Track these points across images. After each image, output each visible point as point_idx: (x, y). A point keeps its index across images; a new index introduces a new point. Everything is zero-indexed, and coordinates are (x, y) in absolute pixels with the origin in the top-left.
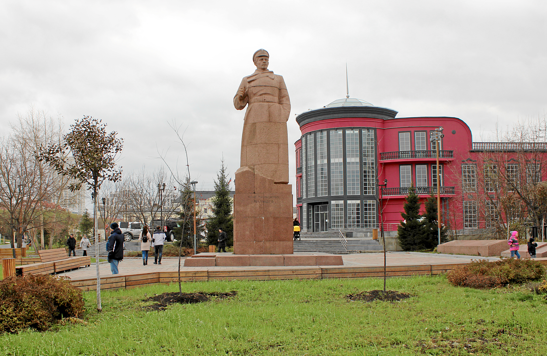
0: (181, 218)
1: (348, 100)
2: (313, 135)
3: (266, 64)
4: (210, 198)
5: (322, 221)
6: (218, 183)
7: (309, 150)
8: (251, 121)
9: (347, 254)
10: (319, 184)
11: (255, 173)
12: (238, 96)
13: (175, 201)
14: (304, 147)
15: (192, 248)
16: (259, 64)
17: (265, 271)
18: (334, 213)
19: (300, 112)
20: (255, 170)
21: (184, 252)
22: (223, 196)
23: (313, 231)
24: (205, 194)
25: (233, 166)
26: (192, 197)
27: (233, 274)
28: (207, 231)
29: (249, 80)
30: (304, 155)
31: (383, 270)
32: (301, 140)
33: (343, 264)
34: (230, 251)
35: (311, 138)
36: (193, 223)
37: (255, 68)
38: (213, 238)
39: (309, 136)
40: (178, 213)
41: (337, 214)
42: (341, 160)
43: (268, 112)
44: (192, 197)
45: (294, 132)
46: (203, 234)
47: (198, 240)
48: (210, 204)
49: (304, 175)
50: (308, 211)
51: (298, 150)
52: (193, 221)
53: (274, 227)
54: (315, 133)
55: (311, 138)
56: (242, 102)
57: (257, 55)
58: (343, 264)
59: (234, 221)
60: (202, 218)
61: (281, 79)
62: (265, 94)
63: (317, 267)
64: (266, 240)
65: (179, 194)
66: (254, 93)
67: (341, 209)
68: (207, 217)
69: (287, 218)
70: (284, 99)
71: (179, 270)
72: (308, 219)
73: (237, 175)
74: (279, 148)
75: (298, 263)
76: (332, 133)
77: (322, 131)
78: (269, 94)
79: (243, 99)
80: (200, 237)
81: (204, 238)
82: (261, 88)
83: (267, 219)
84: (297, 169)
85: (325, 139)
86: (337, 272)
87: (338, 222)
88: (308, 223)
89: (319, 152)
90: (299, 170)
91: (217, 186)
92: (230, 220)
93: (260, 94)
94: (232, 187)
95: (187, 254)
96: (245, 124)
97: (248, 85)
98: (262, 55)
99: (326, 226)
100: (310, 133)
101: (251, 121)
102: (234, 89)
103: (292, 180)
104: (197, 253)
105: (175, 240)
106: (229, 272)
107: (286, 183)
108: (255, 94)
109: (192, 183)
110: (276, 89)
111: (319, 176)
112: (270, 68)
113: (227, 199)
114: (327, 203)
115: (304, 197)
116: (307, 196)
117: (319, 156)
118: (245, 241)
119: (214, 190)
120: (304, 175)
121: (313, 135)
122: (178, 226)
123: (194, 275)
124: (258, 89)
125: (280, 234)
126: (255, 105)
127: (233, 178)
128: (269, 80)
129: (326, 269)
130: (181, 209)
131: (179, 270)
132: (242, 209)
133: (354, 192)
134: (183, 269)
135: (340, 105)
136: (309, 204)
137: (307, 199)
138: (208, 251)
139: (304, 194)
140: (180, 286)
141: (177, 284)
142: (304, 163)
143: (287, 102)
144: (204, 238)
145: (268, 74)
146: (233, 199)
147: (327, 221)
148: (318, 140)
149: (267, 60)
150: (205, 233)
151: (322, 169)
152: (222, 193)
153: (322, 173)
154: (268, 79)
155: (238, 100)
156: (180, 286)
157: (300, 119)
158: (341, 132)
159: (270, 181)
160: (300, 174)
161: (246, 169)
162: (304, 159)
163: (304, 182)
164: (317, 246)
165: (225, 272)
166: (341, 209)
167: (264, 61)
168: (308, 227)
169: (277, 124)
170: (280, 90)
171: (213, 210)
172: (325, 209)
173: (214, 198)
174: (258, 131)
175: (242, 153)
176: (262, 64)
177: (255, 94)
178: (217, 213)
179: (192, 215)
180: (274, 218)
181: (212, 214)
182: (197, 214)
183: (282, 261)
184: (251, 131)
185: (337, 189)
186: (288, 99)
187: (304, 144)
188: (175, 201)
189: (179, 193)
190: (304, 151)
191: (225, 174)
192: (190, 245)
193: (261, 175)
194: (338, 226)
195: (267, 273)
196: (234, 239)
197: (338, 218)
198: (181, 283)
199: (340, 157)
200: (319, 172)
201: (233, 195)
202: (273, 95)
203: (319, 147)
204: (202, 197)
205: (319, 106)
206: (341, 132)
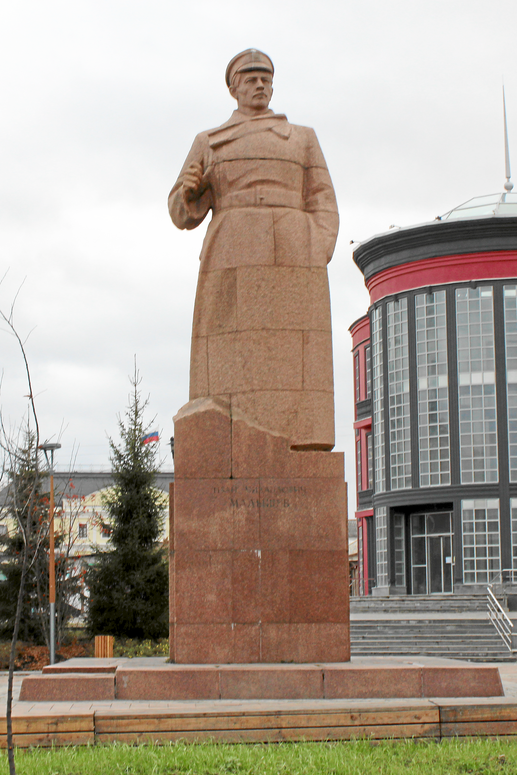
0: (8, 554)
1: (509, 198)
2: (404, 301)
3: (264, 94)
4: (98, 494)
6: (123, 449)
8: (220, 263)
10: (425, 449)
11: (235, 418)
12: (181, 190)
14: (377, 340)
16: (246, 93)
17: (269, 714)
18: (471, 538)
19: (365, 236)
20: (234, 409)
21: (20, 656)
23: (409, 592)
24: (80, 482)
25: (166, 401)
26: (44, 489)
27: (171, 723)
28: (87, 594)
29: (214, 143)
30: (378, 363)
32: (369, 316)
33: (500, 693)
34: (157, 653)
35: (398, 311)
37: (233, 104)
39: (391, 305)
41: (481, 540)
42: (490, 378)
43: (270, 237)
44: (44, 489)
45: (349, 295)
47: (62, 619)
48: (99, 510)
49: (379, 422)
50: (392, 532)
51: (361, 349)
52: (47, 564)
53: (291, 581)
54: (411, 296)
55: (398, 311)
56: (193, 205)
58: (500, 693)
60: (72, 552)
62: (262, 182)
63: (425, 702)
64: (269, 621)
66: (230, 178)
67: (493, 526)
68: (89, 551)
69: (332, 553)
70: (320, 197)
71: (9, 713)
72: (392, 556)
74: (305, 341)
75: (364, 689)
76: (462, 295)
77: (430, 291)
78: (274, 182)
80: (66, 612)
81: (77, 613)
82: (252, 165)
83: (270, 557)
84: (359, 406)
85: (442, 314)
86: (487, 715)
87: (482, 564)
88: (392, 568)
89: (422, 353)
90: (363, 407)
91: (120, 457)
92: (156, 560)
93: (245, 184)
94: (163, 459)
95: (28, 663)
96: (204, 272)
97: (210, 157)
98: (253, 65)
99: (444, 577)
100: (396, 298)
101: (220, 263)
102: (169, 171)
103: (345, 440)
104: (59, 658)
106: (159, 717)
107: (328, 447)
108: (231, 184)
109: (45, 448)
110: (294, 166)
111: (424, 424)
112: (276, 105)
113: (147, 497)
114: (449, 506)
115: (380, 490)
116: (388, 487)
117: (422, 366)
118: (206, 623)
120: (379, 422)
121: (404, 301)
123: (53, 728)
125: (300, 597)
126: (236, 214)
127: (167, 432)
128: (274, 139)
129: (454, 709)
131: (9, 713)
132: (194, 524)
133: (480, 476)
134: (20, 709)
136: (395, 511)
137: (388, 495)
138: (89, 654)
139: (380, 479)
140: (11, 761)
142: (379, 387)
143: (329, 208)
144: (77, 613)
145: (271, 123)
146: (166, 495)
147: (449, 560)
148: (421, 317)
150: (83, 598)
151: (433, 406)
152: (133, 481)
153: (433, 418)
154: (272, 138)
155: (182, 200)
157: (367, 255)
158: (487, 293)
159: (279, 442)
160: (366, 420)
161: (207, 405)
162: (378, 374)
163: (380, 444)
164: (419, 637)
165: (146, 717)
166: (493, 526)
168: (393, 581)
170: (307, 169)
171: (106, 530)
173: (112, 492)
175: (193, 360)
176: (253, 92)
177: (231, 184)
178: (119, 538)
179: (45, 544)
180: (291, 552)
181: (104, 543)
182: (59, 540)
183: (317, 680)
184: (220, 293)
186: (331, 198)
187: (377, 329)
192: (36, 636)
193: (250, 424)
194: (482, 577)
195: (273, 721)
196: (172, 616)
197: (482, 552)
200: (424, 413)
202: (285, 186)
204: (74, 491)
205: (196, 265)
206: (487, 293)
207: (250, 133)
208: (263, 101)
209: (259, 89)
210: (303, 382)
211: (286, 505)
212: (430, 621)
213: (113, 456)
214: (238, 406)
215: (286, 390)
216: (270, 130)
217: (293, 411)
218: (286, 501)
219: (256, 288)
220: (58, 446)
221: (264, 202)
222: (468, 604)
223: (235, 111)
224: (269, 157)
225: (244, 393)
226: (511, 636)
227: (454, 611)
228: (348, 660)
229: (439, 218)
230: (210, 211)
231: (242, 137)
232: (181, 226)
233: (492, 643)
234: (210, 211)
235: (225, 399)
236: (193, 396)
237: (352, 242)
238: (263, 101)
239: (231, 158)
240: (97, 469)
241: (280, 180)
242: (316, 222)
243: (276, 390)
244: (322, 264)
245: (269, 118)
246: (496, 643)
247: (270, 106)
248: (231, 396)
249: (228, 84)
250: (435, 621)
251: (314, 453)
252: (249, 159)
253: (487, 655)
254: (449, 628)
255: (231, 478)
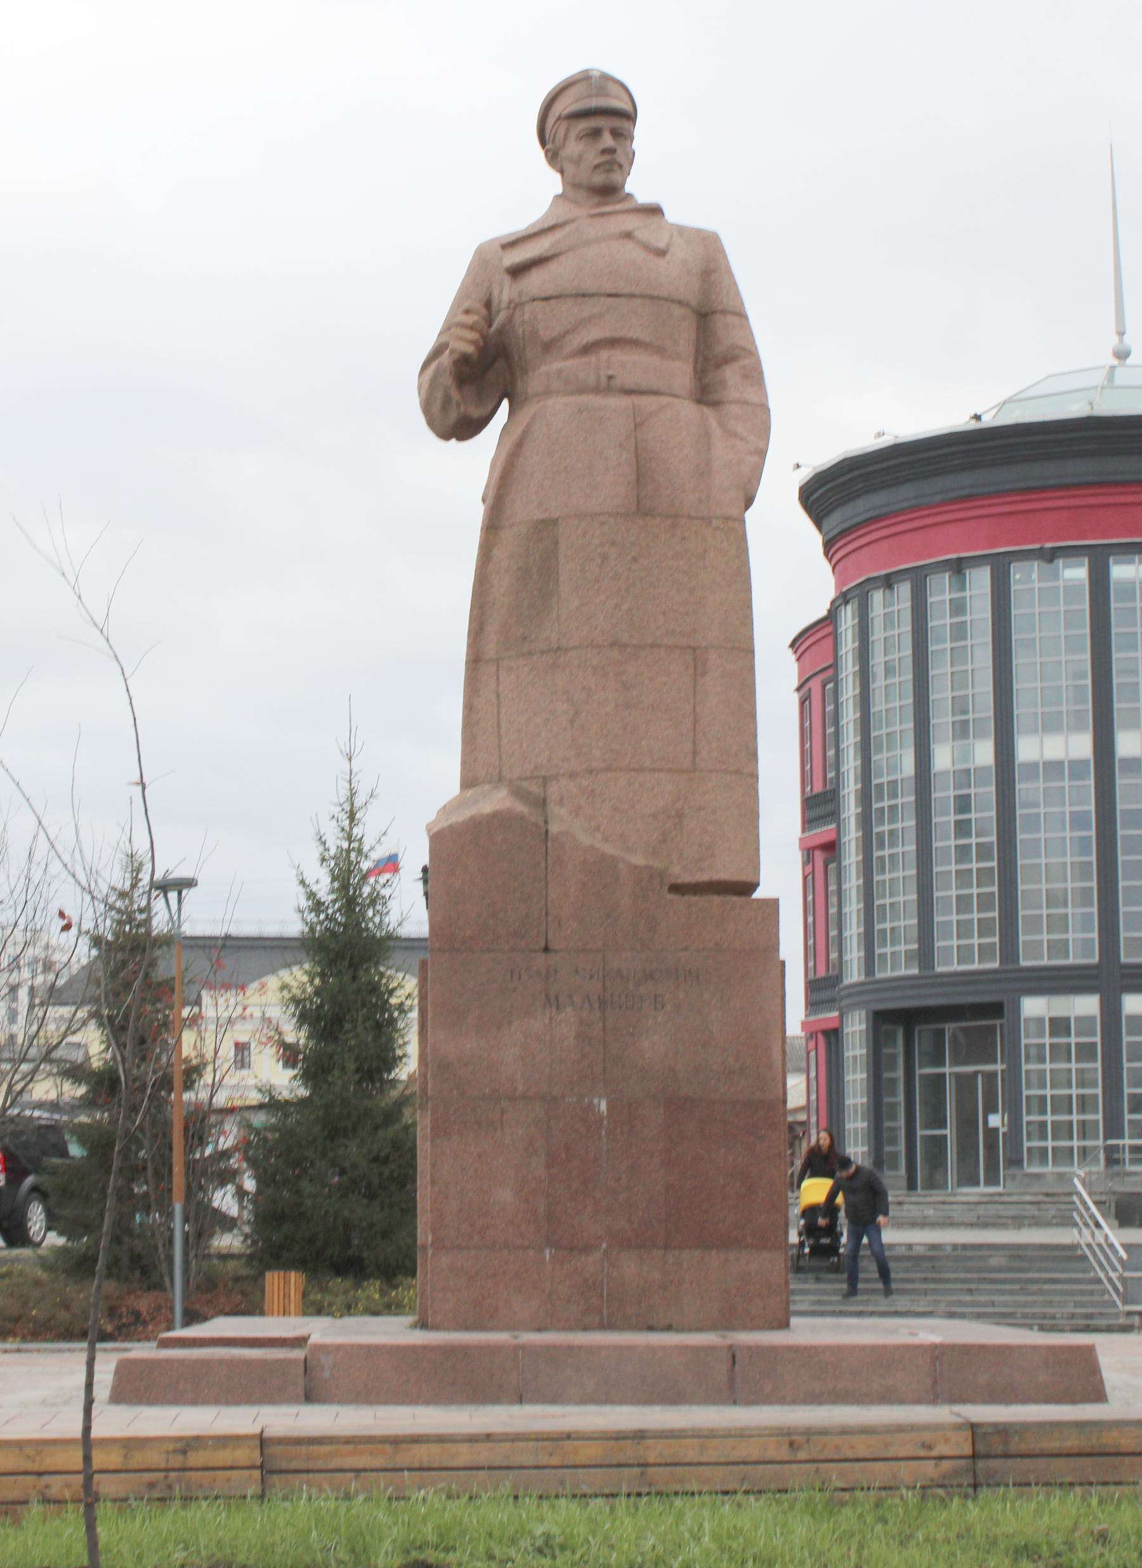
0: (87, 1104)
1: (1121, 377)
2: (904, 590)
4: (273, 982)
5: (967, 1124)
6: (324, 888)
7: (878, 683)
8: (524, 509)
9: (1126, 1329)
10: (946, 892)
11: (554, 828)
12: (445, 359)
13: (54, 996)
14: (849, 668)
15: (158, 1286)
16: (578, 161)
20: (554, 809)
21: (112, 1312)
22: (354, 966)
23: (911, 1185)
24: (236, 957)
25: (416, 785)
28: (250, 1185)
29: (515, 262)
30: (850, 715)
31: (75, 1458)
32: (831, 619)
34: (391, 1308)
35: (891, 610)
36: (166, 1135)
37: (552, 183)
38: (287, 1228)
39: (877, 597)
40: (75, 1072)
42: (1082, 746)
45: (789, 571)
46: (224, 1200)
47: (199, 1236)
48: (275, 1013)
49: (851, 836)
50: (877, 1064)
51: (815, 685)
52: (168, 1124)
54: (919, 579)
55: (891, 610)
57: (565, 106)
58: (1098, 1395)
59: (422, 1123)
60: (220, 1100)
61: (710, 261)
62: (613, 343)
65: (85, 953)
66: (546, 334)
67: (1085, 1052)
68: (254, 1098)
70: (730, 373)
71: (87, 1429)
73: (439, 840)
74: (698, 669)
76: (1026, 578)
77: (958, 567)
78: (635, 343)
79: (475, 376)
80: (210, 1221)
81: (227, 1223)
82: (590, 308)
85: (981, 610)
89: (941, 694)
90: (819, 805)
91: (318, 906)
92: (392, 1115)
93: (579, 351)
94: (406, 910)
95: (126, 1326)
96: (492, 526)
97: (506, 291)
98: (594, 103)
100: (888, 582)
101: (524, 509)
102: (422, 313)
103: (781, 875)
104: (192, 1317)
105: (55, 1240)
107: (747, 888)
108: (548, 347)
110: (677, 311)
111: (945, 842)
112: (640, 185)
113: (374, 988)
114: (995, 1010)
115: (854, 975)
116: (869, 969)
117: (942, 719)
119: (294, 927)
120: (851, 836)
121: (904, 590)
122: (75, 1150)
123: (177, 1461)
124: (568, 312)
126: (555, 411)
127: (416, 855)
128: (638, 255)
129: (1003, 1430)
130: (93, 1044)
131: (87, 1429)
134: (115, 1422)
135: (1075, 409)
136: (885, 1021)
137: (871, 986)
138: (253, 1307)
139: (854, 954)
140: (91, 1528)
141: (73, 1517)
142: (851, 764)
143: (751, 395)
145: (630, 223)
147: (995, 1121)
148: (940, 621)
149: (623, 135)
150: (241, 1193)
152: (344, 951)
153: (962, 828)
154: (630, 252)
155: (448, 381)
156: (91, 1528)
157: (825, 494)
158: (1077, 573)
160: (824, 832)
161: (496, 801)
162: (850, 738)
163: (853, 882)
165: (370, 1440)
166: (1085, 1052)
167: (608, 141)
169: (684, 526)
171: (289, 1055)
172: (979, 1047)
173: (298, 977)
174: (567, 568)
175: (469, 708)
176: (592, 157)
177: (548, 347)
178: (314, 1068)
179: (166, 1083)
182: (192, 1073)
185: (1059, 923)
186: (755, 375)
187: (848, 644)
188: (54, 996)
189: (84, 945)
190: (849, 690)
191: (368, 829)
192: (145, 1271)
193: (585, 840)
195: (629, 1451)
196: (424, 1235)
197: (1062, 1104)
198: (103, 1510)
199: (1078, 727)
200: (944, 819)
201: (415, 959)
202: (659, 350)
203: (940, 671)
205: (477, 513)
206: (1077, 573)
207: (587, 243)
208: (616, 177)
209: (604, 151)
210: (695, 753)
211: (658, 1006)
212: (955, 1247)
213: (304, 903)
214: (561, 803)
215: (659, 770)
216: (628, 235)
217: (673, 813)
218: (659, 999)
219: (599, 561)
220: (190, 883)
221: (616, 383)
222: (1032, 1211)
223: (557, 197)
224: (626, 290)
225: (573, 775)
226: (1121, 1279)
227: (1004, 1226)
228: (784, 1325)
229: (977, 417)
230: (505, 403)
231: (570, 249)
232: (445, 435)
233: (1083, 1293)
234: (505, 403)
235: (534, 788)
236: (468, 782)
237: (798, 466)
238: (616, 177)
239: (549, 293)
240: (271, 929)
241: (647, 339)
242: (722, 424)
243: (641, 769)
244: (735, 512)
245: (627, 211)
246: (1092, 1293)
247: (629, 187)
248: (545, 781)
249: (543, 141)
250: (965, 1247)
251: (717, 899)
252: (584, 295)
253: (1073, 1316)
254: (994, 1262)
255: (546, 949)
